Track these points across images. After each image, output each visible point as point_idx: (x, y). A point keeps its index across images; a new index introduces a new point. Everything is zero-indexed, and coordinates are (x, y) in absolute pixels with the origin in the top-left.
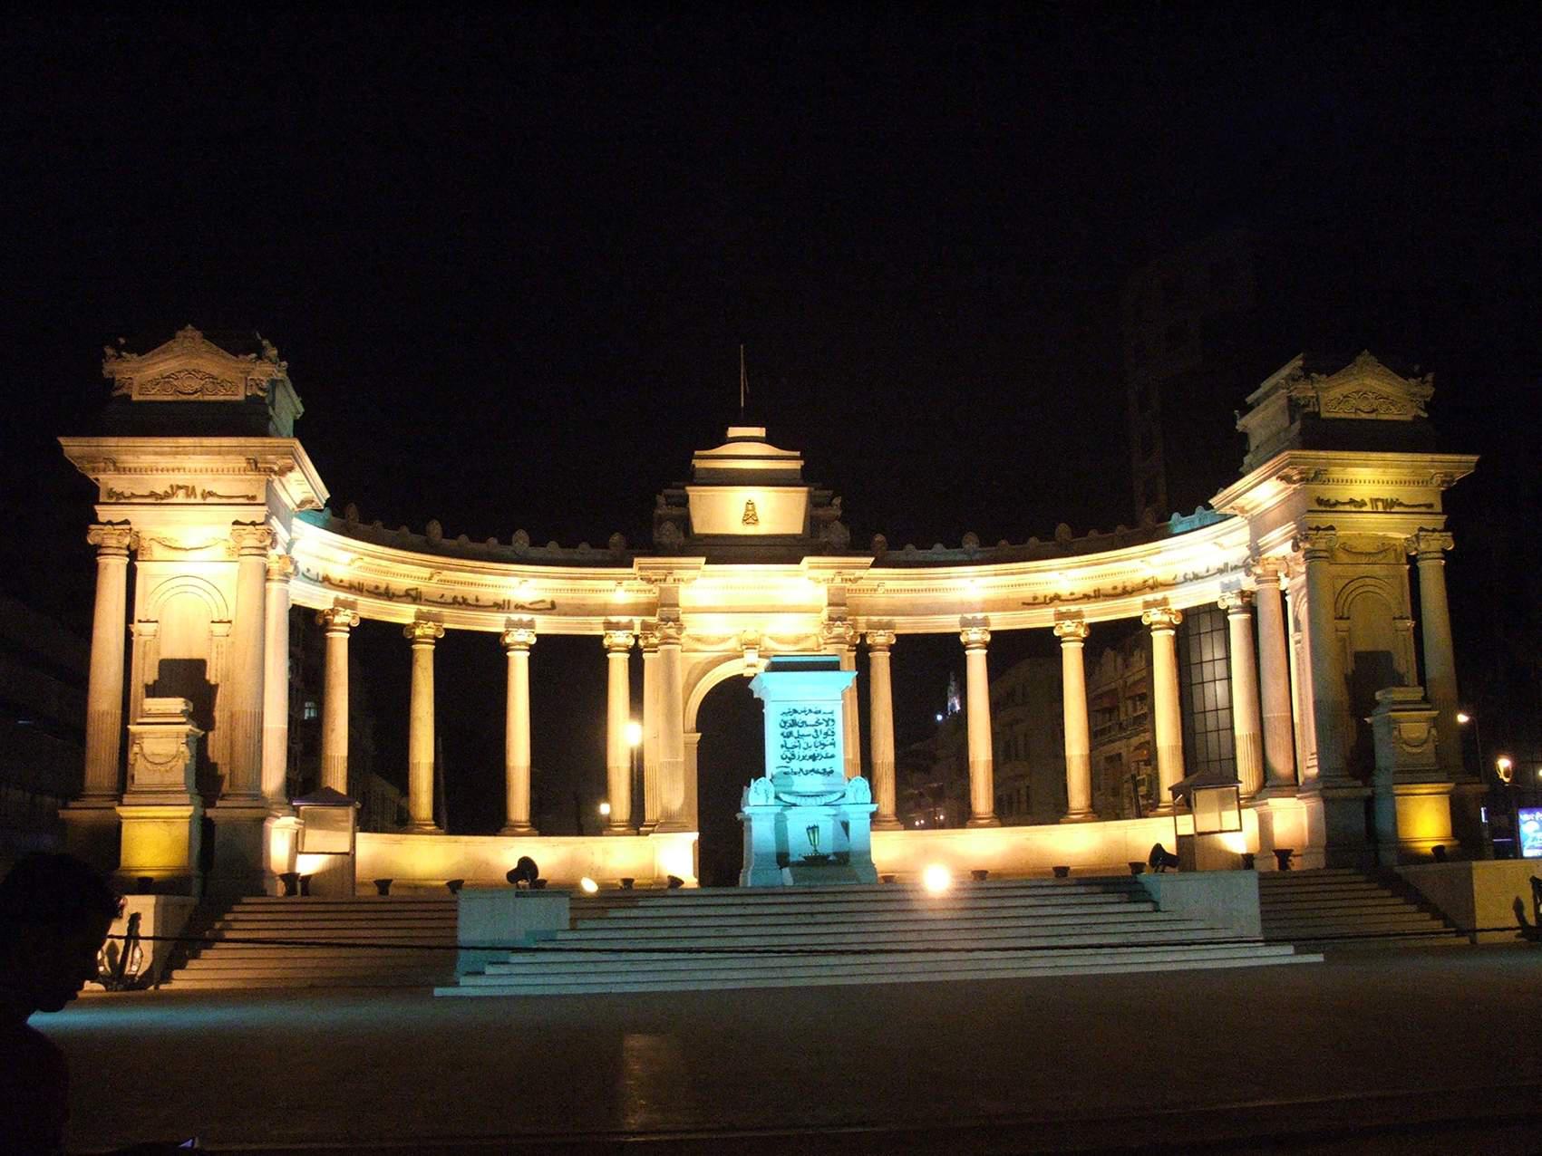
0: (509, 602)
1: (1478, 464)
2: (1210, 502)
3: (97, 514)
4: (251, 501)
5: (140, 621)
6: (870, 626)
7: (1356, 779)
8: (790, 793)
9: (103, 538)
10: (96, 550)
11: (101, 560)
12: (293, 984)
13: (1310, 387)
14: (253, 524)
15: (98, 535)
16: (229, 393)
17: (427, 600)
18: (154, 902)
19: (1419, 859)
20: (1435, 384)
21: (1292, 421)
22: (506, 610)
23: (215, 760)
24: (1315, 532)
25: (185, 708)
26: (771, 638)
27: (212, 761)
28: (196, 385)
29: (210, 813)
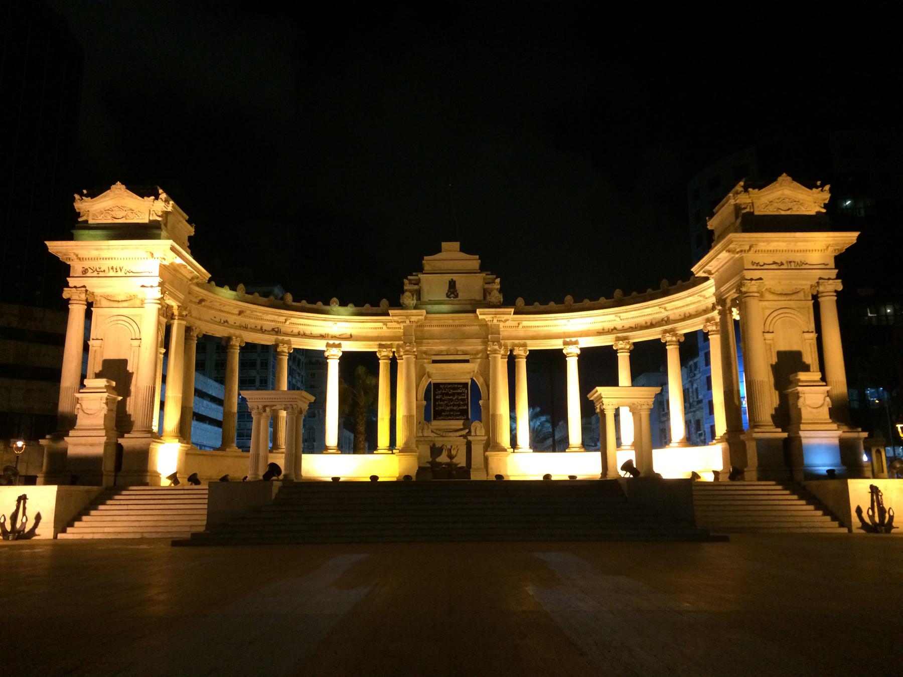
1: (859, 238)
2: (692, 270)
3: (68, 283)
5: (93, 339)
6: (515, 345)
9: (71, 295)
10: (67, 301)
11: (70, 306)
12: (147, 536)
13: (748, 197)
15: (69, 293)
16: (141, 218)
17: (284, 333)
19: (819, 477)
21: (737, 217)
22: (326, 338)
23: (130, 413)
25: (107, 384)
28: (123, 214)
29: (120, 441)
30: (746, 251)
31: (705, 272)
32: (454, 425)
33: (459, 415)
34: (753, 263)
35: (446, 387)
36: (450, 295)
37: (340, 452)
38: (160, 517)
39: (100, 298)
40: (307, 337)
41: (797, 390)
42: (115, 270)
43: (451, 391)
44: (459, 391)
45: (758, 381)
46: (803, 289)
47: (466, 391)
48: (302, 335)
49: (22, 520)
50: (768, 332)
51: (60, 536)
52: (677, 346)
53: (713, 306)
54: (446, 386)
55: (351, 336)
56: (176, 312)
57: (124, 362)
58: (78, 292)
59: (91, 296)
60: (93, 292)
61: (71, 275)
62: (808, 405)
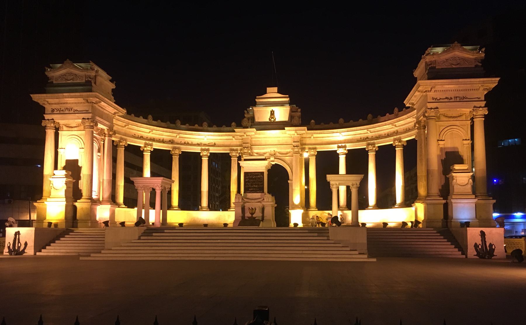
0: (202, 143)
3: (44, 117)
4: (87, 112)
5: (60, 148)
7: (490, 197)
8: (247, 198)
10: (45, 128)
13: (432, 57)
14: (88, 119)
15: (45, 123)
16: (81, 79)
17: (176, 143)
18: (34, 229)
20: (485, 52)
24: (430, 110)
26: (279, 153)
27: (80, 189)
29: (444, 201)
30: (429, 91)
31: (410, 104)
32: (256, 196)
33: (258, 190)
34: (433, 99)
35: (252, 175)
36: (271, 119)
37: (317, 209)
38: (99, 244)
39: (62, 125)
40: (189, 145)
41: (452, 175)
42: (68, 110)
43: (254, 176)
44: (259, 177)
45: (431, 169)
46: (465, 113)
47: (263, 177)
48: (186, 144)
49: (8, 245)
50: (441, 140)
51: (38, 254)
52: (401, 148)
53: (414, 125)
54: (251, 174)
55: (215, 144)
56: (106, 132)
57: (77, 161)
58: (50, 122)
59: (57, 125)
60: (59, 122)
61: (46, 113)
62: (458, 184)
